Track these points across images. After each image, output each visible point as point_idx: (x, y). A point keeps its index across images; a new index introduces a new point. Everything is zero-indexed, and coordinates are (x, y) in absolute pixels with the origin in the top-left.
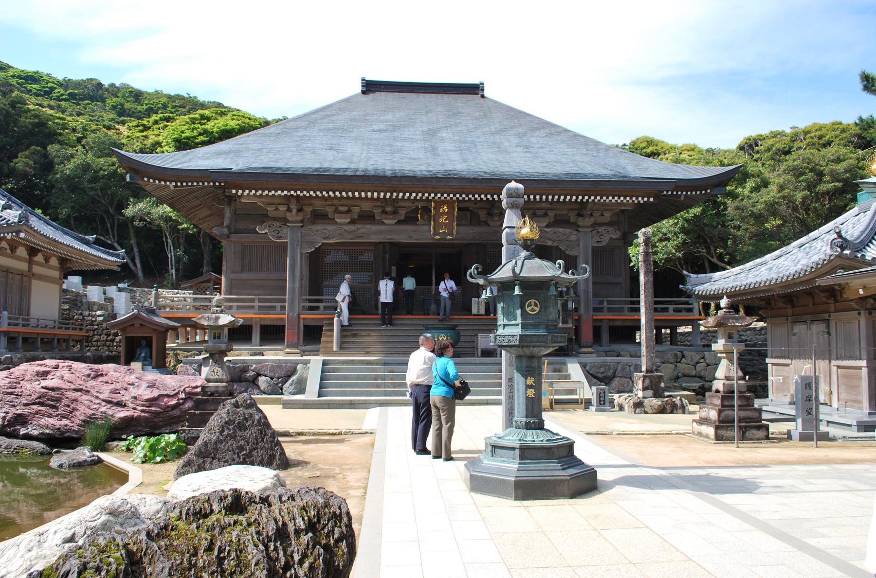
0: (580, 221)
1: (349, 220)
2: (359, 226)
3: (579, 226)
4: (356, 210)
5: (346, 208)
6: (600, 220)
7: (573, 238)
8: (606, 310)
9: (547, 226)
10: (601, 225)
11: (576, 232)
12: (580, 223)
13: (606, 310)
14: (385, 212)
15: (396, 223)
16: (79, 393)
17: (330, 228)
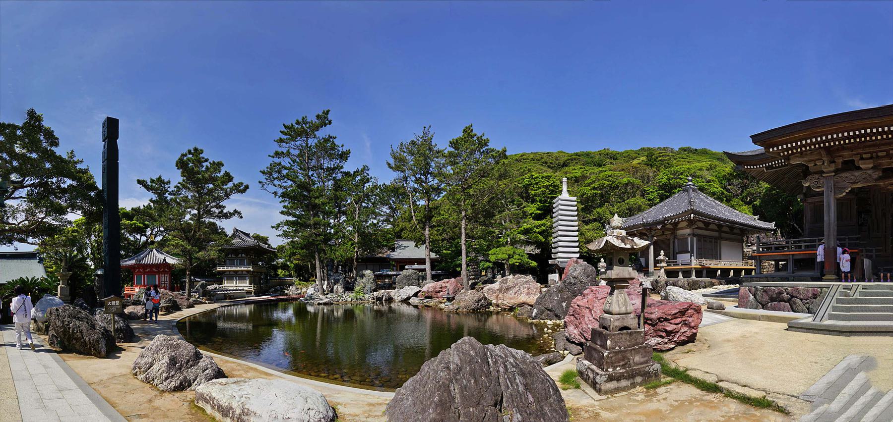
5: (869, 155)
17: (857, 174)
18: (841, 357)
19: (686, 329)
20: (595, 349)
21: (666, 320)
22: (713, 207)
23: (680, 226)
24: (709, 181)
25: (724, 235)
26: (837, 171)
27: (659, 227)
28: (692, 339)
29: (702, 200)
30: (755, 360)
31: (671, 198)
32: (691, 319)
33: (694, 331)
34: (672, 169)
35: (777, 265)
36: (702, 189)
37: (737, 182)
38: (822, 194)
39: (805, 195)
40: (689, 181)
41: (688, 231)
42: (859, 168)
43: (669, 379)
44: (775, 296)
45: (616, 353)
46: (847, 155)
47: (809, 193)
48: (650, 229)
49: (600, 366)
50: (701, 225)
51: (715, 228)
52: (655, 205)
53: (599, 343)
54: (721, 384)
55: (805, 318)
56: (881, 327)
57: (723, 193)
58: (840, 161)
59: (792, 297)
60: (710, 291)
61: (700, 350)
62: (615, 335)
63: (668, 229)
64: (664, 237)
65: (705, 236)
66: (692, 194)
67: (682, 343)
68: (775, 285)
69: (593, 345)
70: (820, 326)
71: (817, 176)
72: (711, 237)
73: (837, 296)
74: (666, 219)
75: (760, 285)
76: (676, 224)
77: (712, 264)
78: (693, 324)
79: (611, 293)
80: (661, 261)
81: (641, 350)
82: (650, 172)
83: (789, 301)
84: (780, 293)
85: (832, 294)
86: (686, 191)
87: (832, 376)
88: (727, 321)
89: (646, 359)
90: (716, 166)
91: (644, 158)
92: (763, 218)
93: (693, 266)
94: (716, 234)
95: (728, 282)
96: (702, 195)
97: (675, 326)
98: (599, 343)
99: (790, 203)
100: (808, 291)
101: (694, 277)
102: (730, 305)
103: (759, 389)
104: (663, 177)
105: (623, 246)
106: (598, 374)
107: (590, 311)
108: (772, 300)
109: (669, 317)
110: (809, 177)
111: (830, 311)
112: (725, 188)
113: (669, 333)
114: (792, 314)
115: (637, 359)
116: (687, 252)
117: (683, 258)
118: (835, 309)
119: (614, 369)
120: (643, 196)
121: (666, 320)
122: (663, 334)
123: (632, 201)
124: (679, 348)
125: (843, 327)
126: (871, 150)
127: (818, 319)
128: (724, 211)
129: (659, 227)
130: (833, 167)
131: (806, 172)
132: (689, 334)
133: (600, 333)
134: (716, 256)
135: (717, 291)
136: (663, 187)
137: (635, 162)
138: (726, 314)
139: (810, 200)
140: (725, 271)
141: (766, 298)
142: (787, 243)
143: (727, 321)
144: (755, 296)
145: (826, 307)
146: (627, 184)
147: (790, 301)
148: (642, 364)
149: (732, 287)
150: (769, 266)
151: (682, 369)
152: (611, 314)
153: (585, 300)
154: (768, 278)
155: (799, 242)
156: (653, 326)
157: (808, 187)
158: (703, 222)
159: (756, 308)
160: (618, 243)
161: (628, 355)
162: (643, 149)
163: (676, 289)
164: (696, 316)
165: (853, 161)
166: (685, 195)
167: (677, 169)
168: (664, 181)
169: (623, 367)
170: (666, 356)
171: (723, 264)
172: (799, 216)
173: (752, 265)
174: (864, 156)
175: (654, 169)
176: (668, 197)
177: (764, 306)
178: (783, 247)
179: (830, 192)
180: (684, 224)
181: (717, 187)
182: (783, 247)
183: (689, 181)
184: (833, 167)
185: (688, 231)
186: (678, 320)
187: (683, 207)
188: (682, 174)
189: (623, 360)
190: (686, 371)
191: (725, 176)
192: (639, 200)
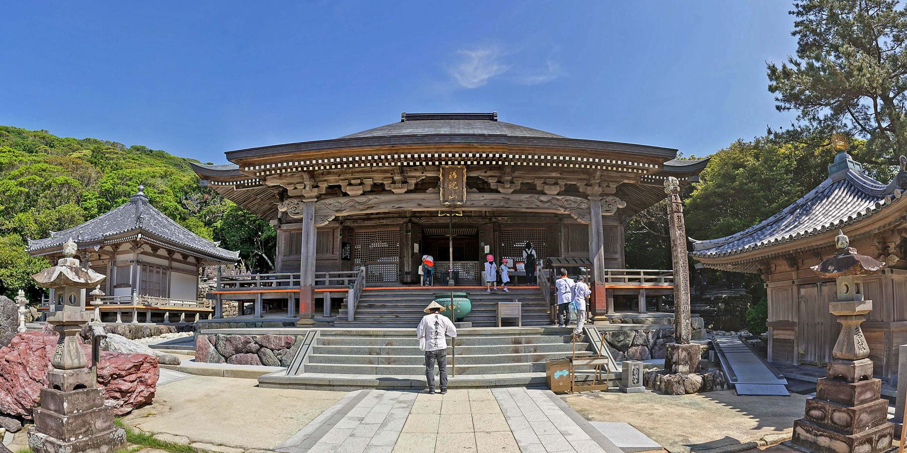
0: (589, 190)
1: (361, 192)
2: (370, 197)
3: (588, 196)
4: (369, 182)
5: (359, 181)
6: (608, 190)
7: (584, 206)
8: (291, 284)
9: (558, 194)
10: (608, 195)
11: (586, 201)
12: (589, 192)
13: (291, 284)
14: (394, 182)
15: (406, 192)
16: (400, 399)
17: (343, 200)
18: (319, 411)
19: (142, 387)
20: (50, 416)
21: (120, 376)
22: (164, 226)
23: (122, 248)
24: (162, 192)
25: (174, 264)
26: (319, 197)
27: (97, 248)
28: (148, 401)
29: (153, 216)
30: (225, 419)
31: (114, 211)
32: (147, 376)
33: (152, 390)
34: (120, 172)
35: (241, 307)
36: (151, 202)
37: (196, 196)
38: (301, 221)
39: (280, 220)
40: (140, 190)
41: (131, 256)
42: (345, 195)
43: (135, 446)
44: (240, 346)
45: (76, 417)
46: (333, 180)
47: (284, 220)
48: (85, 251)
49: (60, 436)
50: (148, 249)
51: (165, 254)
52: (93, 217)
53: (52, 407)
54: (194, 445)
55: (277, 372)
56: (344, 380)
57: (177, 209)
58: (324, 186)
59: (261, 346)
60: (157, 340)
61: (161, 413)
62: (70, 395)
63: (107, 253)
64: (100, 263)
65: (152, 265)
66: (142, 208)
67: (140, 406)
68: (240, 333)
69: (45, 411)
70: (295, 379)
71: (296, 201)
72: (159, 266)
73: (314, 344)
74: (106, 238)
75: (222, 332)
76: (116, 246)
77: (158, 303)
78: (150, 382)
79: (61, 341)
80: (96, 297)
81: (102, 414)
82: (93, 171)
83: (257, 352)
84: (247, 342)
85: (308, 342)
86: (134, 202)
87: (309, 429)
88: (184, 379)
89: (108, 424)
90: (172, 173)
91: (88, 152)
92: (225, 245)
93: (135, 306)
94: (165, 263)
95: (180, 329)
96: (153, 210)
97: (130, 385)
98: (52, 407)
99: (260, 228)
100: (280, 339)
101: (135, 321)
102: (185, 359)
103: (236, 447)
104: (107, 181)
105: (76, 279)
106: (60, 446)
107: (25, 368)
108: (238, 351)
109: (123, 373)
110: (286, 202)
111: (306, 362)
112: (180, 202)
113: (124, 393)
114: (261, 368)
115: (99, 424)
116: (128, 285)
117: (122, 293)
118: (311, 359)
119: (77, 438)
120: (78, 202)
121: (120, 376)
122: (118, 395)
123: (64, 208)
124: (136, 412)
125: (320, 380)
126: (361, 175)
127: (293, 372)
128: (177, 233)
129: (97, 248)
130: (315, 192)
131: (283, 195)
132: (146, 393)
133: (53, 395)
134: (165, 293)
135: (166, 340)
136: (105, 194)
137: (75, 155)
138: (182, 370)
139: (284, 227)
140: (175, 315)
141: (230, 349)
142: (253, 278)
143: (184, 379)
144: (216, 346)
145: (302, 357)
146: (63, 185)
147: (258, 352)
148: (104, 430)
149: (184, 335)
150: (231, 308)
151: (148, 434)
152: (63, 368)
153: (16, 353)
154: (230, 324)
155: (268, 278)
156: (105, 384)
157: (285, 213)
158: (182, 254)
159: (218, 362)
160: (72, 276)
161: (89, 419)
162: (88, 140)
163: (116, 337)
164: (152, 371)
165: (339, 187)
166: (132, 208)
167: (126, 172)
168: (108, 186)
169: (85, 433)
170: (126, 421)
171: (173, 304)
172: (270, 245)
173: (208, 305)
174: (353, 182)
175: (98, 169)
176: (108, 208)
177: (227, 359)
178: (250, 284)
179: (310, 219)
180: (126, 246)
181: (170, 201)
182: (250, 284)
183: (140, 190)
184: (315, 192)
185: (131, 256)
186: (133, 377)
187: (129, 225)
188: (131, 179)
189: (84, 426)
190: (153, 434)
191: (182, 188)
192: (72, 208)
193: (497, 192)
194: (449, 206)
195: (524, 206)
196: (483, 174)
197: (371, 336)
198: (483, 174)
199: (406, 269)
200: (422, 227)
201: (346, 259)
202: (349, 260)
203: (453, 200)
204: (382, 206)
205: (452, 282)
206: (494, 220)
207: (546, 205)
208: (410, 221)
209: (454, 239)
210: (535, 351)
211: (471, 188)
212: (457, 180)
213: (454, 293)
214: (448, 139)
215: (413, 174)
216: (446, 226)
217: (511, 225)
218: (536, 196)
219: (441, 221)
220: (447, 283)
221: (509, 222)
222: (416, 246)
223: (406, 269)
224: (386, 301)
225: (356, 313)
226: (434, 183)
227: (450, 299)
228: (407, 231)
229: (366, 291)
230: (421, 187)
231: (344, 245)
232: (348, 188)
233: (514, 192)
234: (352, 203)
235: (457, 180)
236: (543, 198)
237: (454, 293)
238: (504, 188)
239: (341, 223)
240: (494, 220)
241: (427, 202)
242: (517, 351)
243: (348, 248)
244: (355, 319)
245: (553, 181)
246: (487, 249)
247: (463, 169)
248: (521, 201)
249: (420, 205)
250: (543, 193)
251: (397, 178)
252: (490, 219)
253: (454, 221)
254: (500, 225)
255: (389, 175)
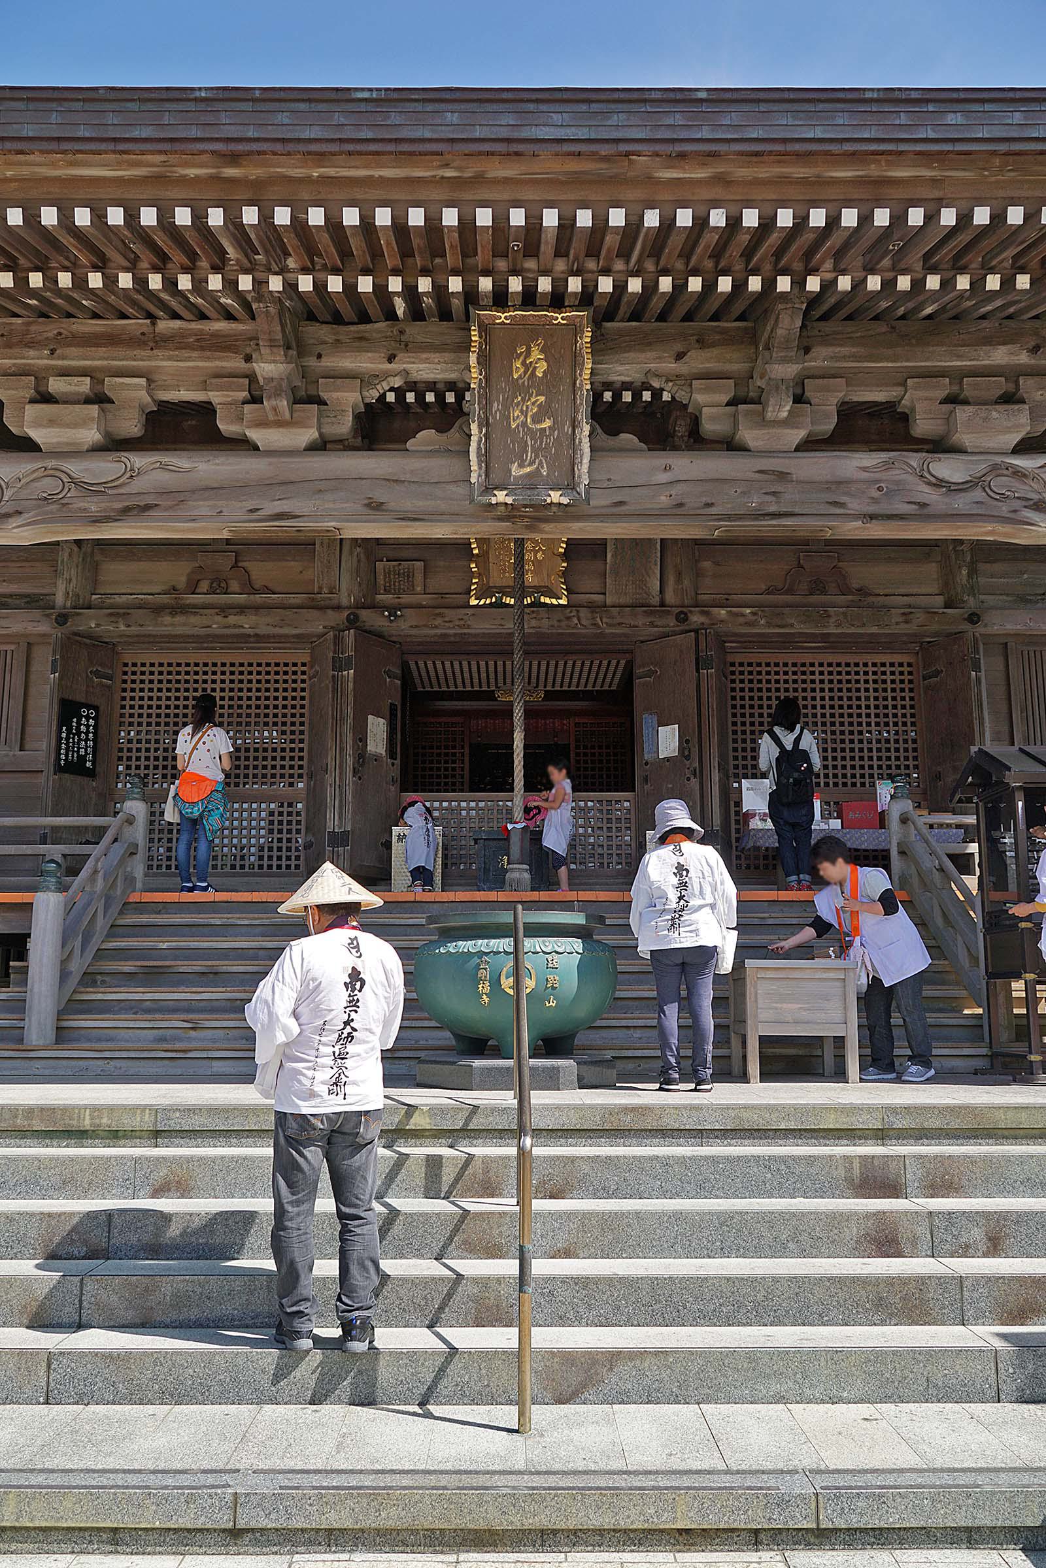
4: (134, 395)
5: (84, 385)
126: (97, 359)
174: (56, 385)
193: (731, 445)
194: (510, 513)
195: (854, 505)
196: (670, 366)
197: (80, 1135)
198: (670, 366)
199: (332, 822)
200: (403, 653)
201: (76, 768)
202: (91, 774)
203: (531, 483)
204: (203, 507)
205: (520, 873)
206: (696, 619)
207: (961, 503)
208: (353, 621)
209: (529, 713)
210: (994, 1247)
211: (613, 432)
212: (548, 385)
213: (527, 917)
214: (503, 123)
215: (347, 362)
216: (499, 648)
217: (764, 642)
218: (914, 459)
219: (482, 627)
220: (498, 880)
221: (762, 627)
222: (377, 728)
223: (332, 822)
224: (225, 954)
225: (70, 1007)
226: (445, 412)
227: (505, 944)
228: (339, 665)
229: (141, 907)
230: (379, 426)
231: (68, 711)
232: (31, 410)
233: (809, 445)
234: (49, 486)
235: (548, 385)
236: (948, 468)
237: (527, 917)
238: (762, 421)
239: (62, 619)
240: (696, 619)
241: (415, 496)
242: (885, 1239)
243: (87, 724)
244: (62, 1035)
245: (1000, 385)
246: (668, 741)
247: (574, 329)
248: (841, 483)
249: (375, 507)
250: (940, 446)
251: (269, 368)
252: (682, 618)
253: (531, 624)
254: (720, 642)
255: (235, 363)
